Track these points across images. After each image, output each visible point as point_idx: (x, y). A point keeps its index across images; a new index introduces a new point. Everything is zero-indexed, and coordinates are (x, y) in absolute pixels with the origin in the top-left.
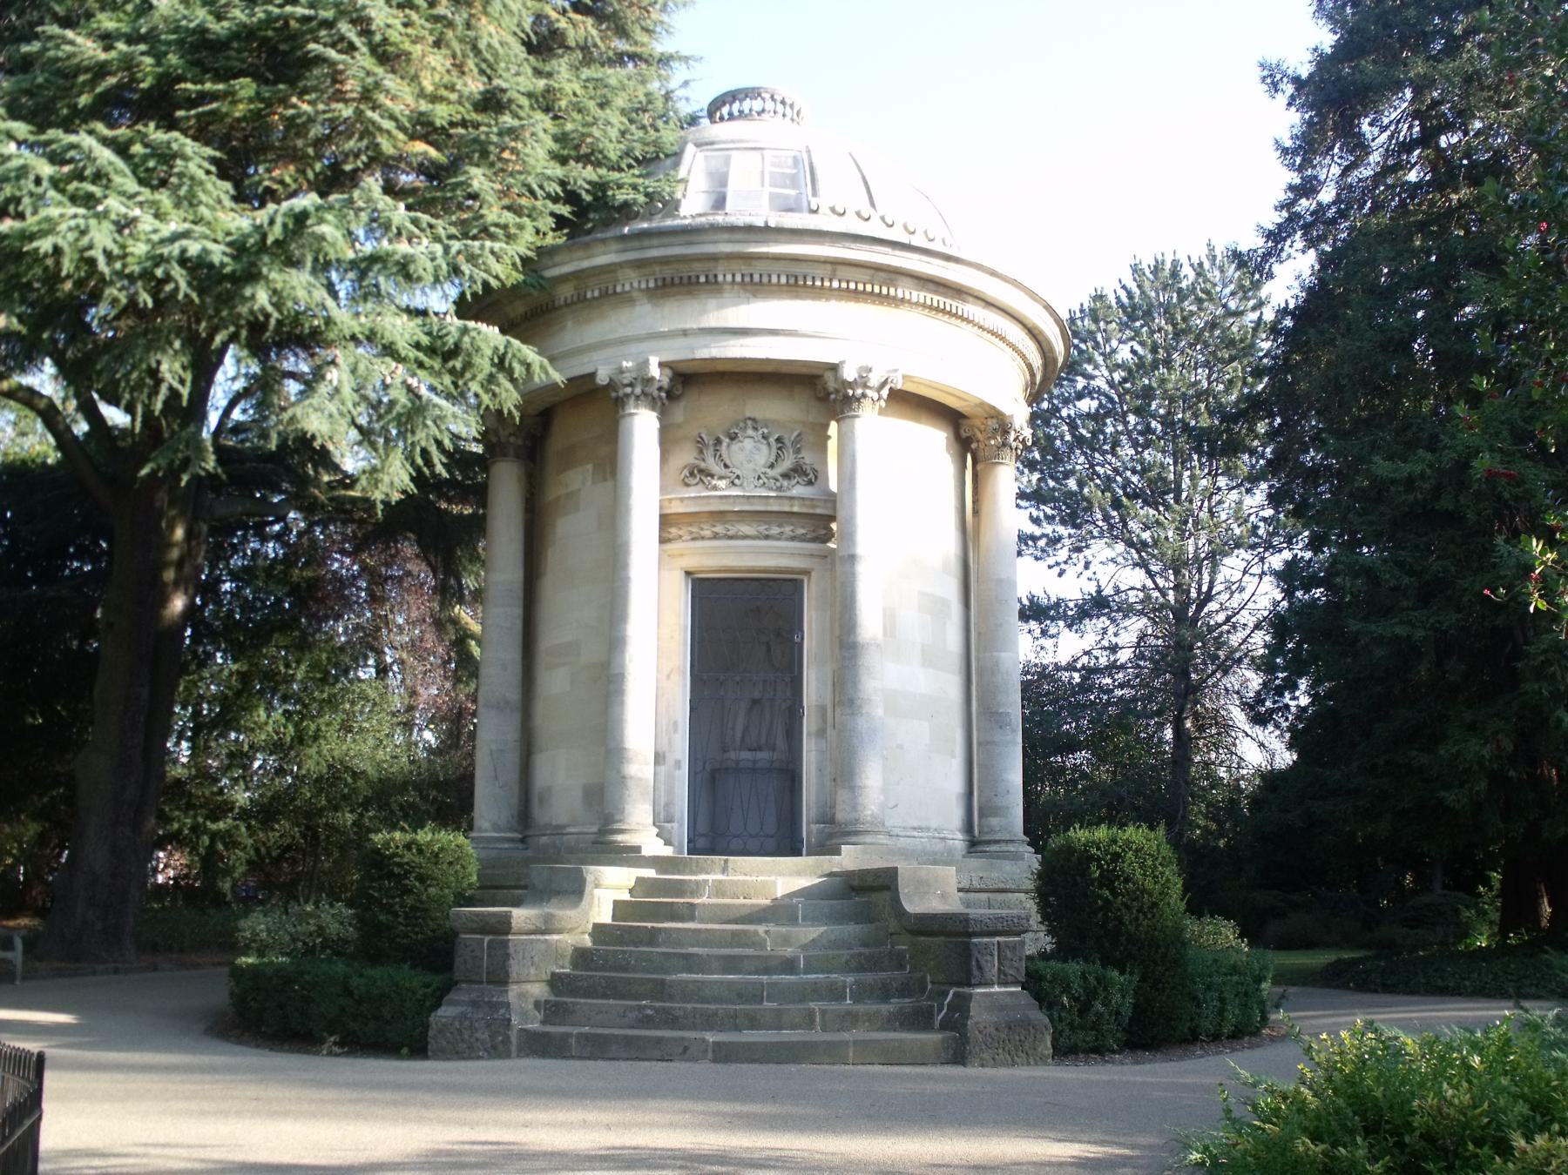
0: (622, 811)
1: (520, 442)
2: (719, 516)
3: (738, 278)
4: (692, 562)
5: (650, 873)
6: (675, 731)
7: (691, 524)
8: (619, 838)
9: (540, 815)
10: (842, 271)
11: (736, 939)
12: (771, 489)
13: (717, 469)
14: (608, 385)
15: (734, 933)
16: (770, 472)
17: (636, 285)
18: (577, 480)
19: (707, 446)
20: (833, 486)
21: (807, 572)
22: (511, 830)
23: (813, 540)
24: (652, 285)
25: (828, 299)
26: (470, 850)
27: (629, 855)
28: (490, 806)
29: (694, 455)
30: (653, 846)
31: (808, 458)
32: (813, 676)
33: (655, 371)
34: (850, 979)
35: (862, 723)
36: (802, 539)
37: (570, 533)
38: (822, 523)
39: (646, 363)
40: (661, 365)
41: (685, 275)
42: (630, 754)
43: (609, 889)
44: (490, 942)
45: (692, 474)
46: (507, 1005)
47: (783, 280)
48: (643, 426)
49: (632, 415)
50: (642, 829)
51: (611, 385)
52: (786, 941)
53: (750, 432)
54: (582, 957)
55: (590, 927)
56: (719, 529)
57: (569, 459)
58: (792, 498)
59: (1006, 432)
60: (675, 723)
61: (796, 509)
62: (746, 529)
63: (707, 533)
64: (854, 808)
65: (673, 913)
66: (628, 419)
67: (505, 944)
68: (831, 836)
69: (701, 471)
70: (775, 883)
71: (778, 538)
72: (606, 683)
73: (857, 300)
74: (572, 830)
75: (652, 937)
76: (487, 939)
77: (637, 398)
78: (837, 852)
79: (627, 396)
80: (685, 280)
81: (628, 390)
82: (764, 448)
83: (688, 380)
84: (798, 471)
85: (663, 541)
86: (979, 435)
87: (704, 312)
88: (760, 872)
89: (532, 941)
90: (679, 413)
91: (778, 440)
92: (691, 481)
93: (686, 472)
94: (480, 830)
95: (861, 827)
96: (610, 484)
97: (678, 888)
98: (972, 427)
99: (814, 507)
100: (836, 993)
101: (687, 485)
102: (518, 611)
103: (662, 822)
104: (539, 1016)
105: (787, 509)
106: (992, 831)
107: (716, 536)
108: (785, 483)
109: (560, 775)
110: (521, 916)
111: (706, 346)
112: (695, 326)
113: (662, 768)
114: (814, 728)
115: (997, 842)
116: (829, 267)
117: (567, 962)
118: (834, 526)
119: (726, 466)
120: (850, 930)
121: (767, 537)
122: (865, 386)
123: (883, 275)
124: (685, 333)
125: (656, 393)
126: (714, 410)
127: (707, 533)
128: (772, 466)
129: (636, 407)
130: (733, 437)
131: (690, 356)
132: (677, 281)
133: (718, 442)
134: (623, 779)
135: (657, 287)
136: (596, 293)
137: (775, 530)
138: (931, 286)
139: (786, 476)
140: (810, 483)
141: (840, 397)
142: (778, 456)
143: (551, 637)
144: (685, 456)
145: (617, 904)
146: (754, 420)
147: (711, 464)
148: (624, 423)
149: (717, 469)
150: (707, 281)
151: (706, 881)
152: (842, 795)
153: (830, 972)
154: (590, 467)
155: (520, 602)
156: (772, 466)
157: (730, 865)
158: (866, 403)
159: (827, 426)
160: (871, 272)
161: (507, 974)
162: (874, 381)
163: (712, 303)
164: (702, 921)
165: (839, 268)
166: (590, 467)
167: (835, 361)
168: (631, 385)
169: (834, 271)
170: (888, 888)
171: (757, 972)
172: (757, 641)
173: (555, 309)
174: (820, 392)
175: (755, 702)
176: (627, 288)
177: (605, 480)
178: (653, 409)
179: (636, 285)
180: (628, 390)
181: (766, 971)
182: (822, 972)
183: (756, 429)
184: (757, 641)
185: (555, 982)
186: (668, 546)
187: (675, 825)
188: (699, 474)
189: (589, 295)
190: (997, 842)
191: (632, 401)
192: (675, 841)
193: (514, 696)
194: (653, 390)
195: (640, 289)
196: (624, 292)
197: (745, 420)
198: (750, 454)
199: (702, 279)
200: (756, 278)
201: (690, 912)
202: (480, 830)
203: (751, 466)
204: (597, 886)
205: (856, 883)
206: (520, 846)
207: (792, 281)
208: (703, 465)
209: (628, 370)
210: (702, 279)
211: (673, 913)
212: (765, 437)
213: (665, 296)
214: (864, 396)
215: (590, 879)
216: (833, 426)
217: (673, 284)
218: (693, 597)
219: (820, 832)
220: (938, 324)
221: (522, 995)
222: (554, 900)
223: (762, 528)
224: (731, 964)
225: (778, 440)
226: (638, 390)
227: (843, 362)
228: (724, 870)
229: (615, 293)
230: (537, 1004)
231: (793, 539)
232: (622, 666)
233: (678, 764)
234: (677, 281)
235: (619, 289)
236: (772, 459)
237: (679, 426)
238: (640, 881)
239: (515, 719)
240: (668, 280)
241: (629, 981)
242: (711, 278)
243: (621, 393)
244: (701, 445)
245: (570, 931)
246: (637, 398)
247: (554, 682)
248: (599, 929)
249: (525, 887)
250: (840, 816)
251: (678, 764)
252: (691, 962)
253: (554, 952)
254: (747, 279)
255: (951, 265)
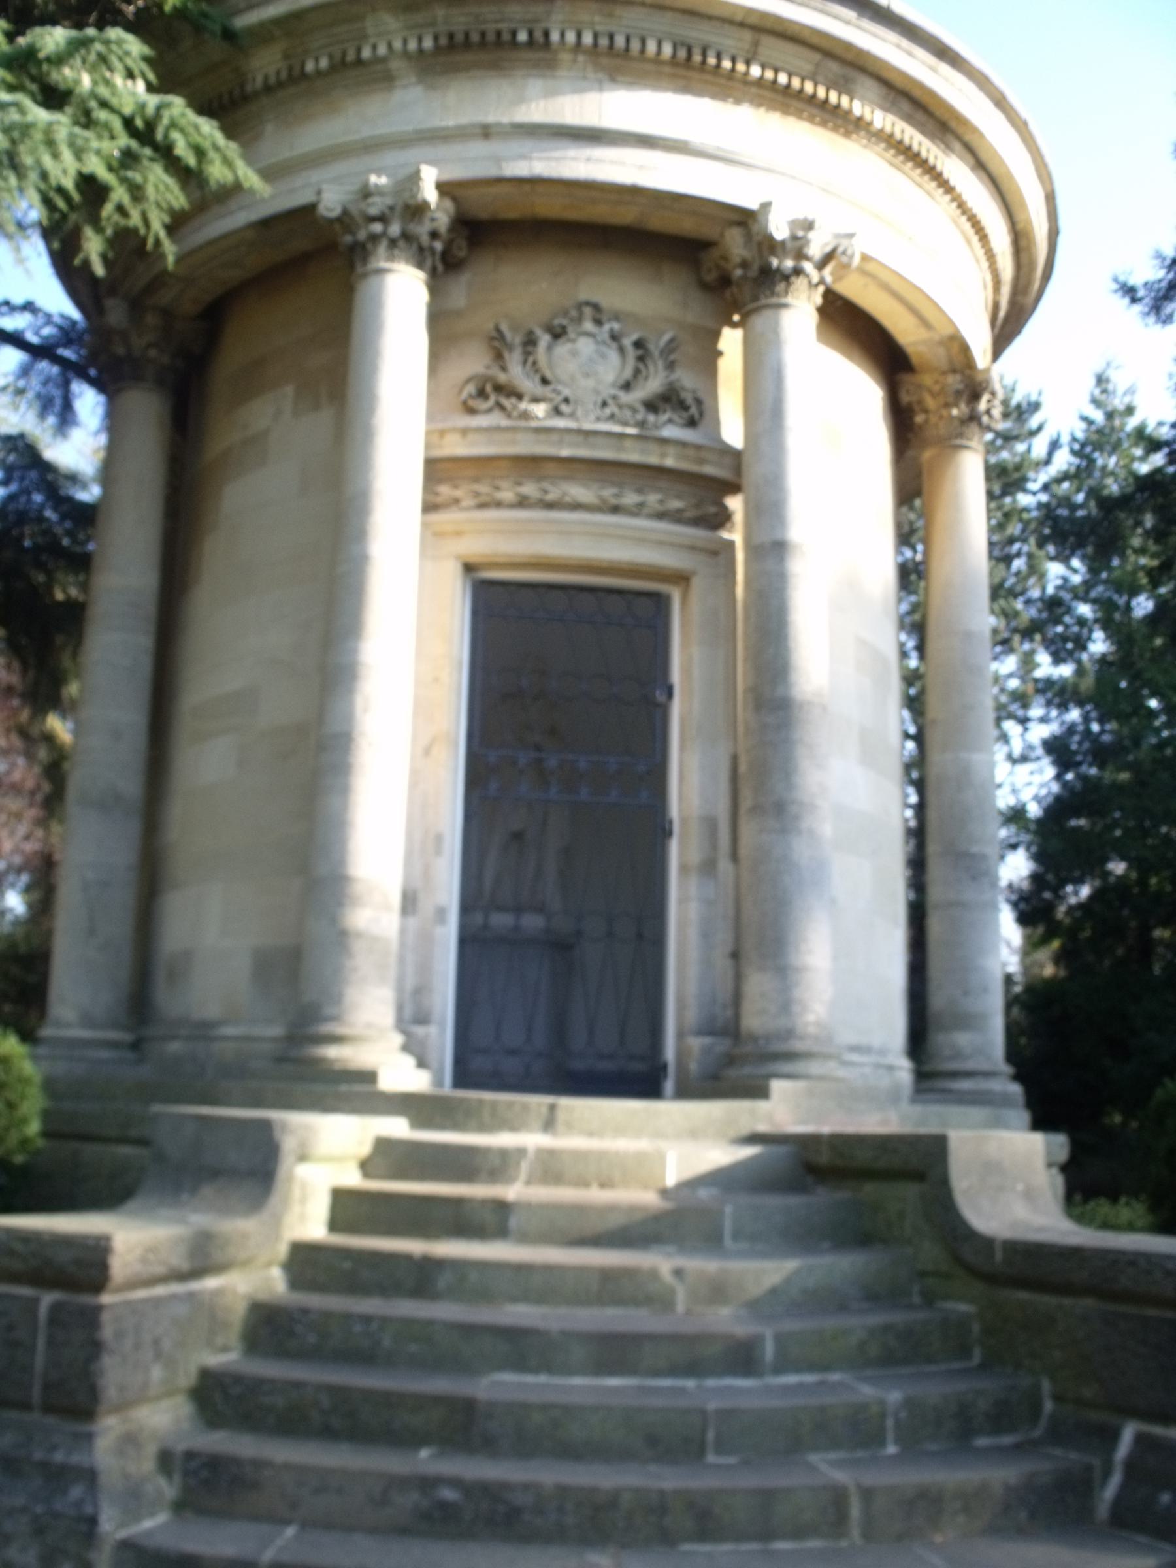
0: (338, 999)
1: (166, 360)
2: (529, 465)
3: (588, 39)
4: (478, 546)
5: (398, 1127)
6: (438, 851)
7: (476, 480)
8: (332, 1052)
9: (171, 1002)
10: (771, 48)
11: (611, 1287)
12: (625, 424)
13: (528, 385)
14: (339, 220)
15: (607, 1275)
16: (625, 398)
17: (398, 45)
18: (266, 424)
19: (510, 348)
20: (733, 432)
21: (682, 579)
22: (115, 1025)
23: (696, 522)
24: (428, 43)
25: (738, 101)
26: (28, 1068)
27: (354, 1091)
28: (77, 993)
29: (486, 366)
30: (401, 1075)
31: (687, 379)
32: (694, 761)
33: (430, 195)
34: (894, 1396)
35: (801, 850)
36: (676, 517)
37: (253, 505)
38: (710, 487)
39: (415, 177)
40: (443, 188)
41: (490, 28)
42: (358, 889)
43: (327, 1156)
44: (56, 1308)
45: (482, 394)
46: (90, 1476)
47: (667, 50)
48: (401, 296)
49: (381, 271)
50: (384, 1033)
51: (345, 220)
52: (717, 1291)
53: (588, 326)
54: (268, 1326)
55: (283, 1250)
56: (530, 489)
57: (251, 383)
58: (664, 441)
59: (975, 397)
60: (439, 839)
61: (670, 462)
62: (579, 492)
63: (507, 495)
64: (786, 1006)
65: (460, 1220)
66: (373, 280)
67: (91, 1317)
68: (731, 1060)
69: (499, 388)
70: (661, 1158)
71: (637, 511)
72: (314, 758)
73: (786, 110)
74: (229, 1031)
75: (423, 1277)
76: (48, 1299)
77: (393, 243)
78: (759, 1091)
79: (374, 238)
80: (491, 37)
81: (377, 227)
82: (613, 356)
83: (482, 234)
84: (667, 400)
85: (429, 507)
86: (930, 402)
87: (521, 100)
88: (620, 1131)
89: (157, 1302)
90: (459, 292)
91: (638, 344)
92: (483, 405)
93: (471, 389)
94: (58, 1024)
95: (798, 1046)
96: (326, 415)
97: (463, 1163)
98: (920, 386)
99: (702, 461)
100: (860, 1432)
101: (472, 411)
102: (144, 641)
103: (412, 1018)
104: (169, 1490)
105: (653, 460)
106: (958, 1055)
107: (523, 503)
108: (651, 418)
109: (213, 932)
110: (132, 1238)
111: (523, 157)
112: (505, 120)
113: (412, 922)
114: (695, 857)
115: (969, 1074)
116: (747, 35)
117: (233, 1336)
118: (735, 503)
119: (545, 381)
120: (841, 1266)
121: (615, 509)
122: (800, 255)
123: (834, 67)
124: (486, 132)
125: (425, 240)
126: (524, 287)
127: (507, 495)
128: (627, 386)
129: (391, 258)
130: (558, 334)
131: (491, 171)
132: (475, 37)
133: (530, 342)
134: (342, 938)
135: (437, 48)
136: (324, 63)
137: (630, 499)
138: (906, 106)
139: (651, 406)
140: (692, 423)
141: (754, 272)
142: (637, 372)
143: (204, 684)
144: (472, 362)
145: (341, 1198)
146: (596, 307)
147: (516, 373)
148: (364, 289)
149: (528, 385)
150: (531, 43)
151: (521, 1152)
152: (757, 984)
153: (825, 1368)
154: (289, 390)
155: (152, 628)
156: (627, 386)
157: (561, 1116)
158: (800, 283)
159: (716, 335)
160: (817, 57)
161: (94, 1394)
162: (816, 250)
163: (535, 85)
164: (524, 1238)
165: (767, 41)
166: (289, 390)
167: (752, 204)
168: (382, 219)
169: (756, 44)
170: (919, 1176)
171: (674, 1371)
172: (583, 707)
173: (246, 98)
174: (715, 263)
175: (518, 836)
176: (382, 50)
177: (317, 407)
178: (420, 265)
179: (398, 45)
180: (377, 227)
181: (693, 1369)
182: (812, 1367)
183: (598, 322)
184: (583, 707)
185: (215, 1397)
186: (435, 517)
187: (433, 1030)
188: (493, 392)
189: (310, 66)
190: (969, 1074)
191: (382, 249)
192: (432, 1057)
193: (131, 786)
194: (422, 230)
195: (406, 54)
196: (377, 60)
197: (580, 306)
198: (588, 367)
199: (522, 36)
200: (620, 41)
201: (495, 1220)
202: (58, 1024)
203: (590, 383)
204: (303, 1158)
205: (824, 1158)
206: (130, 1055)
207: (682, 54)
208: (502, 378)
209: (379, 191)
210: (522, 36)
211: (460, 1220)
212: (614, 337)
213: (454, 69)
214: (798, 271)
215: (288, 1144)
216: (731, 341)
217: (467, 44)
218: (475, 613)
219: (706, 1051)
220: (903, 184)
221: (130, 1441)
222: (207, 1191)
223: (608, 493)
224: (614, 1352)
225: (638, 344)
226: (395, 229)
227: (766, 206)
228: (549, 1124)
229: (359, 62)
230: (165, 1460)
231: (661, 516)
232: (349, 718)
233: (441, 913)
234: (475, 37)
235: (366, 53)
236: (628, 373)
237: (459, 314)
238: (383, 1146)
239: (133, 828)
240: (460, 38)
241: (389, 1400)
242: (539, 36)
243: (362, 235)
244: (498, 347)
245: (245, 1264)
246: (393, 243)
247: (207, 763)
248: (305, 1261)
249: (142, 1142)
250: (752, 1022)
251: (441, 913)
252: (521, 1348)
253: (207, 1312)
254: (604, 42)
255: (944, 68)
